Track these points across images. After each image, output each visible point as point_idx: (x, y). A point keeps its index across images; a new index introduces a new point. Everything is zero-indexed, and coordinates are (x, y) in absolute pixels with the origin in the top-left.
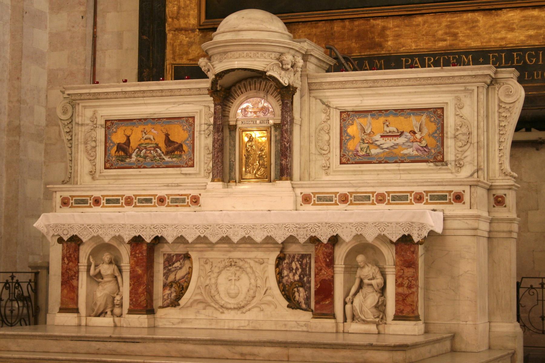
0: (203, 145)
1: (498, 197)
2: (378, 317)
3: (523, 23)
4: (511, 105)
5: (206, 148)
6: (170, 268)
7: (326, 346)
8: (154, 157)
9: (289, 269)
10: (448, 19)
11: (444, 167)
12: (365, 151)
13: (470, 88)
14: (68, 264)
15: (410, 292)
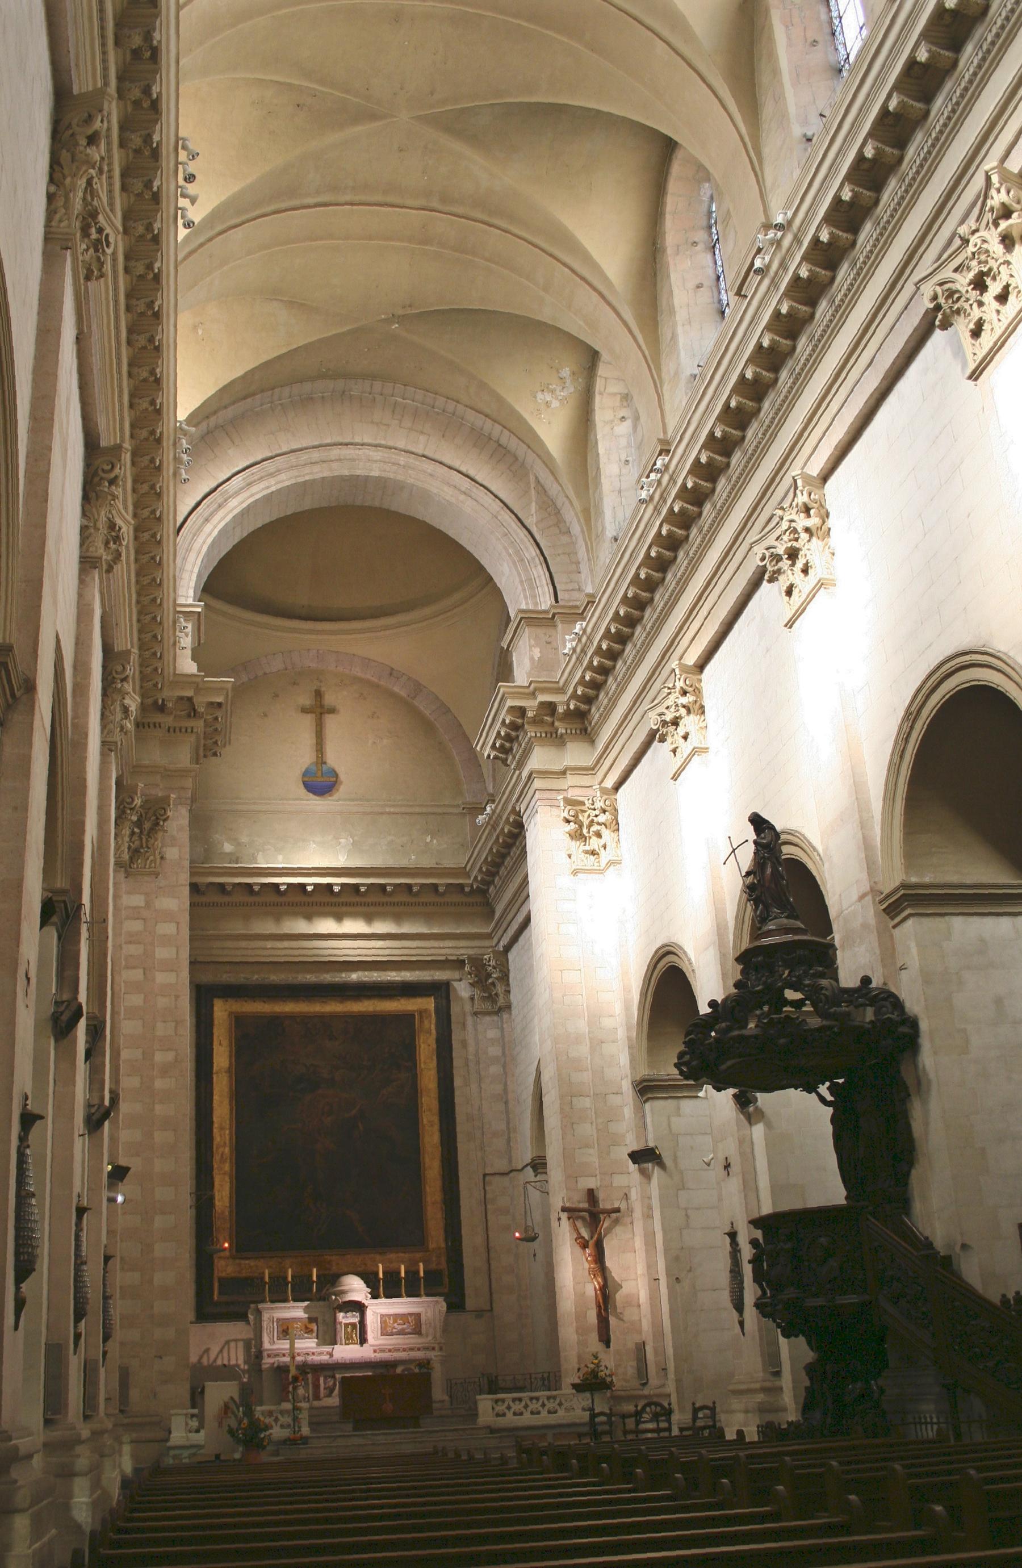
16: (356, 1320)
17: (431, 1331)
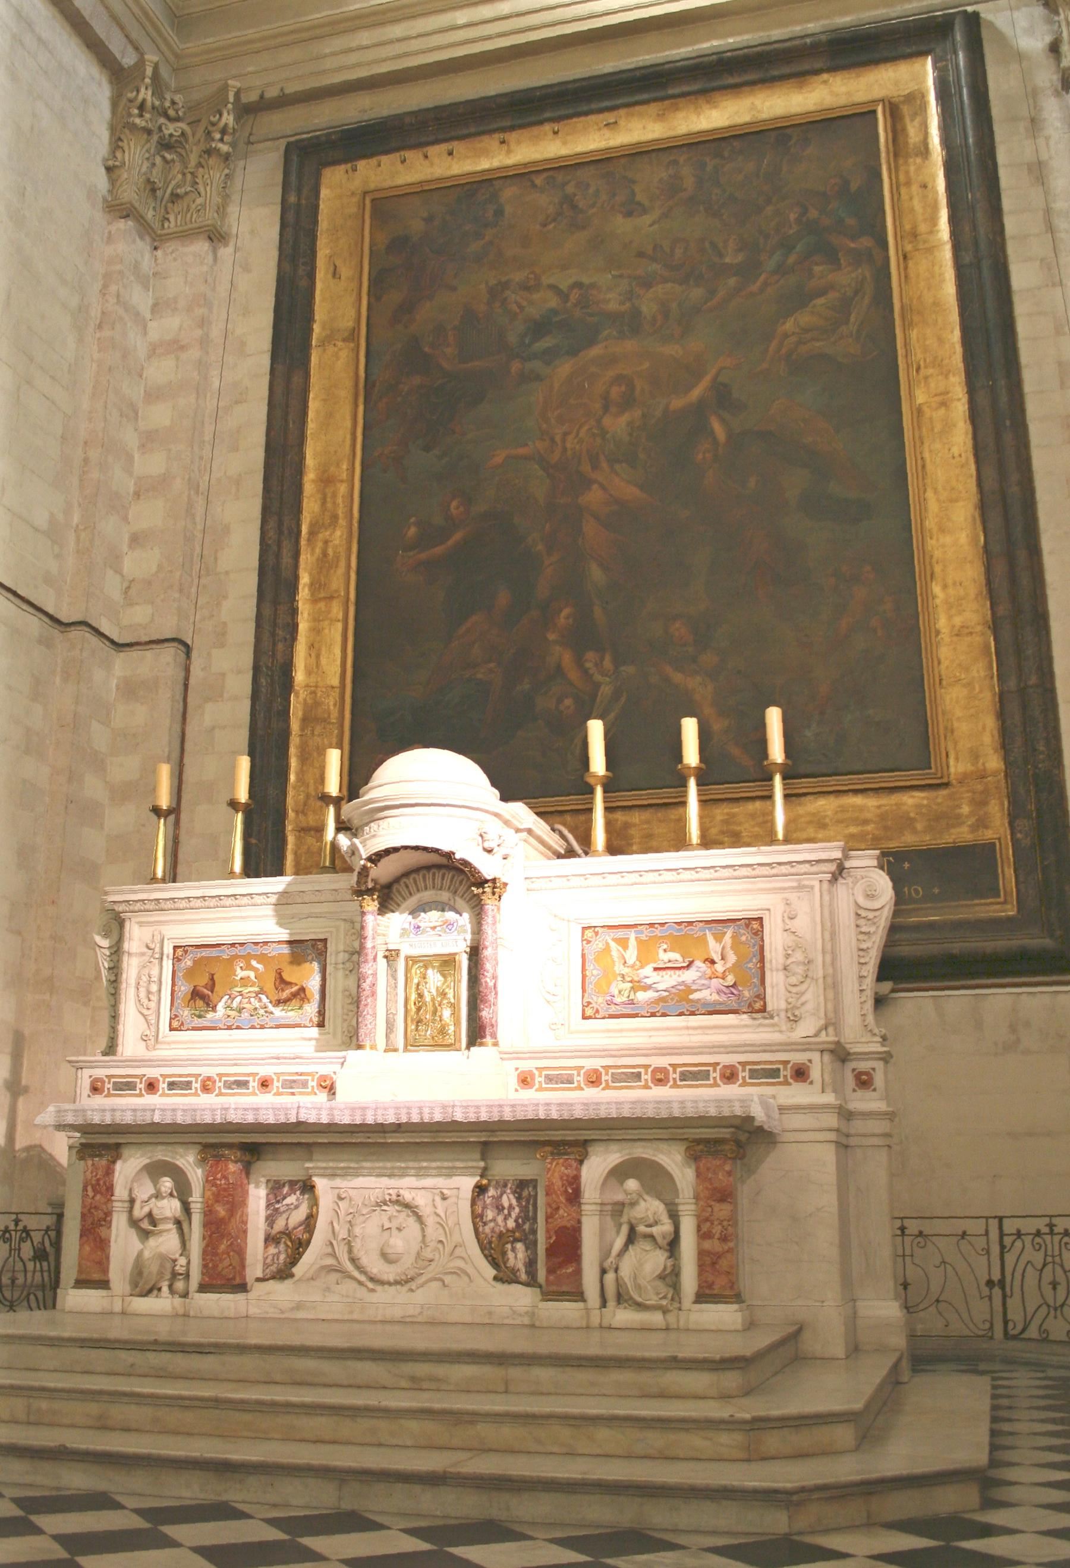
0: (340, 988)
1: (861, 1073)
2: (664, 1297)
3: (840, 816)
4: (877, 913)
5: (347, 993)
6: (277, 1206)
7: (584, 1363)
8: (256, 1009)
9: (497, 1208)
10: (726, 811)
11: (767, 1021)
12: (626, 994)
13: (806, 883)
14: (93, 1198)
15: (726, 1248)
16: (159, 874)
17: (813, 997)
